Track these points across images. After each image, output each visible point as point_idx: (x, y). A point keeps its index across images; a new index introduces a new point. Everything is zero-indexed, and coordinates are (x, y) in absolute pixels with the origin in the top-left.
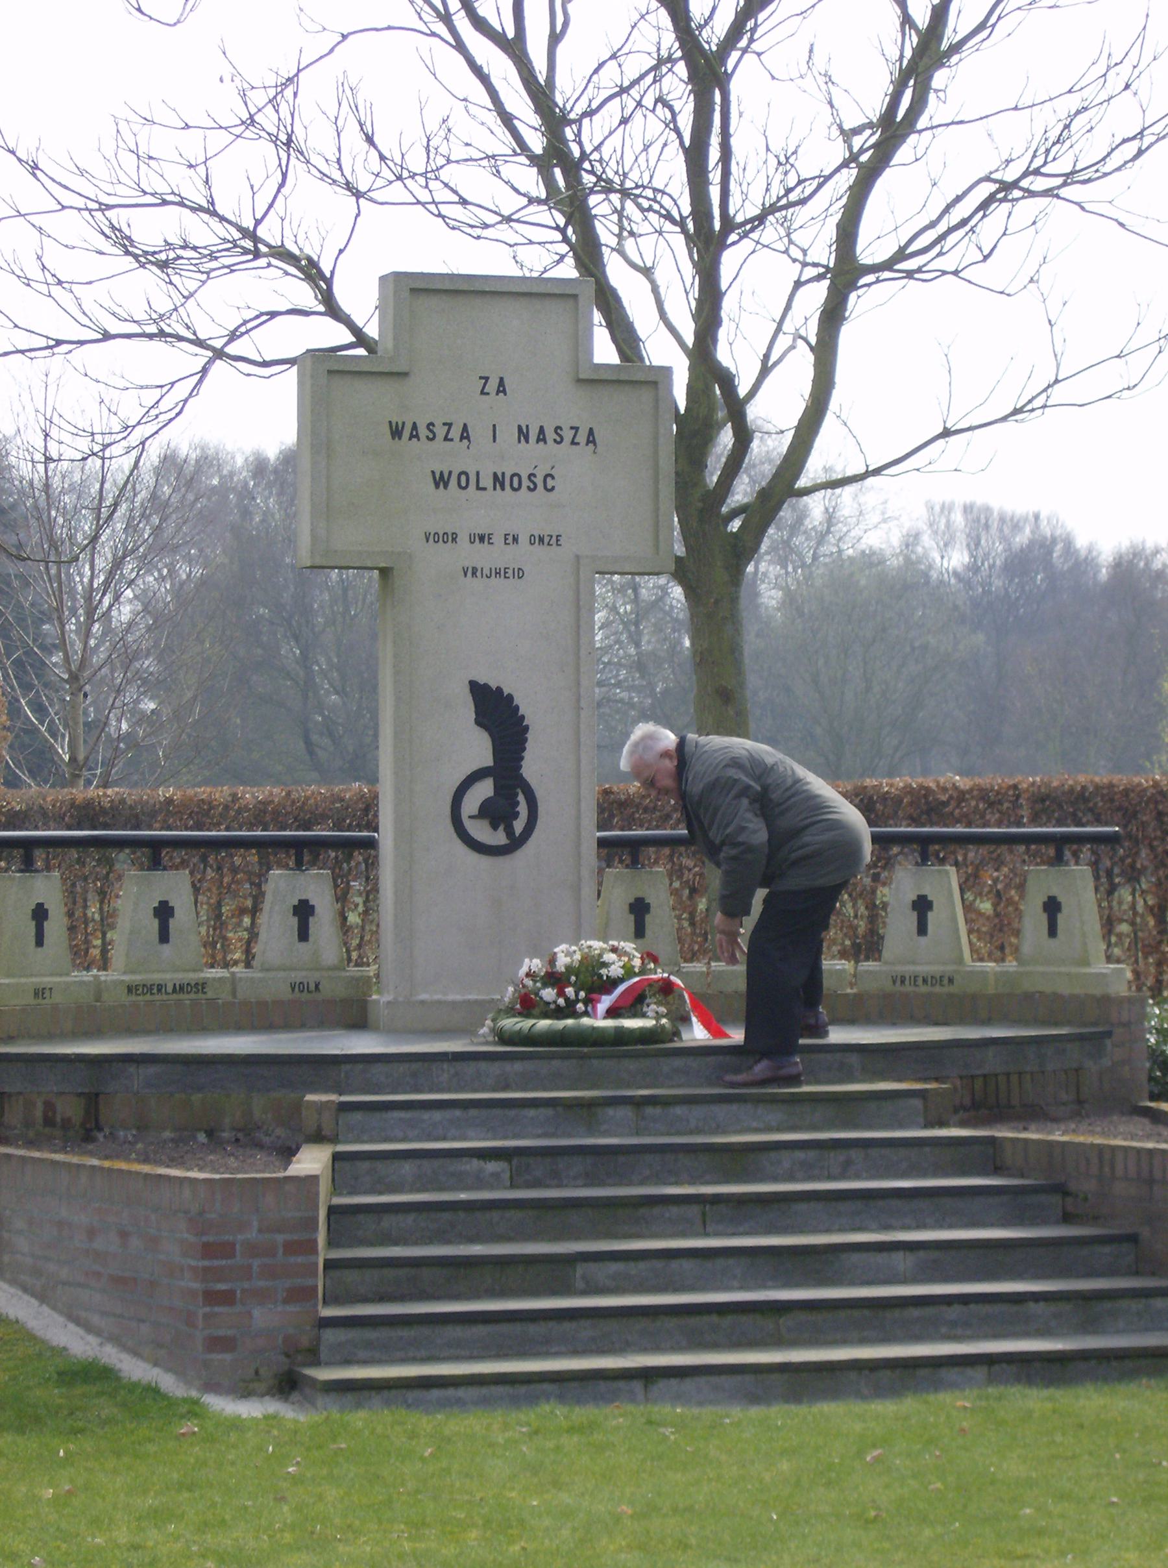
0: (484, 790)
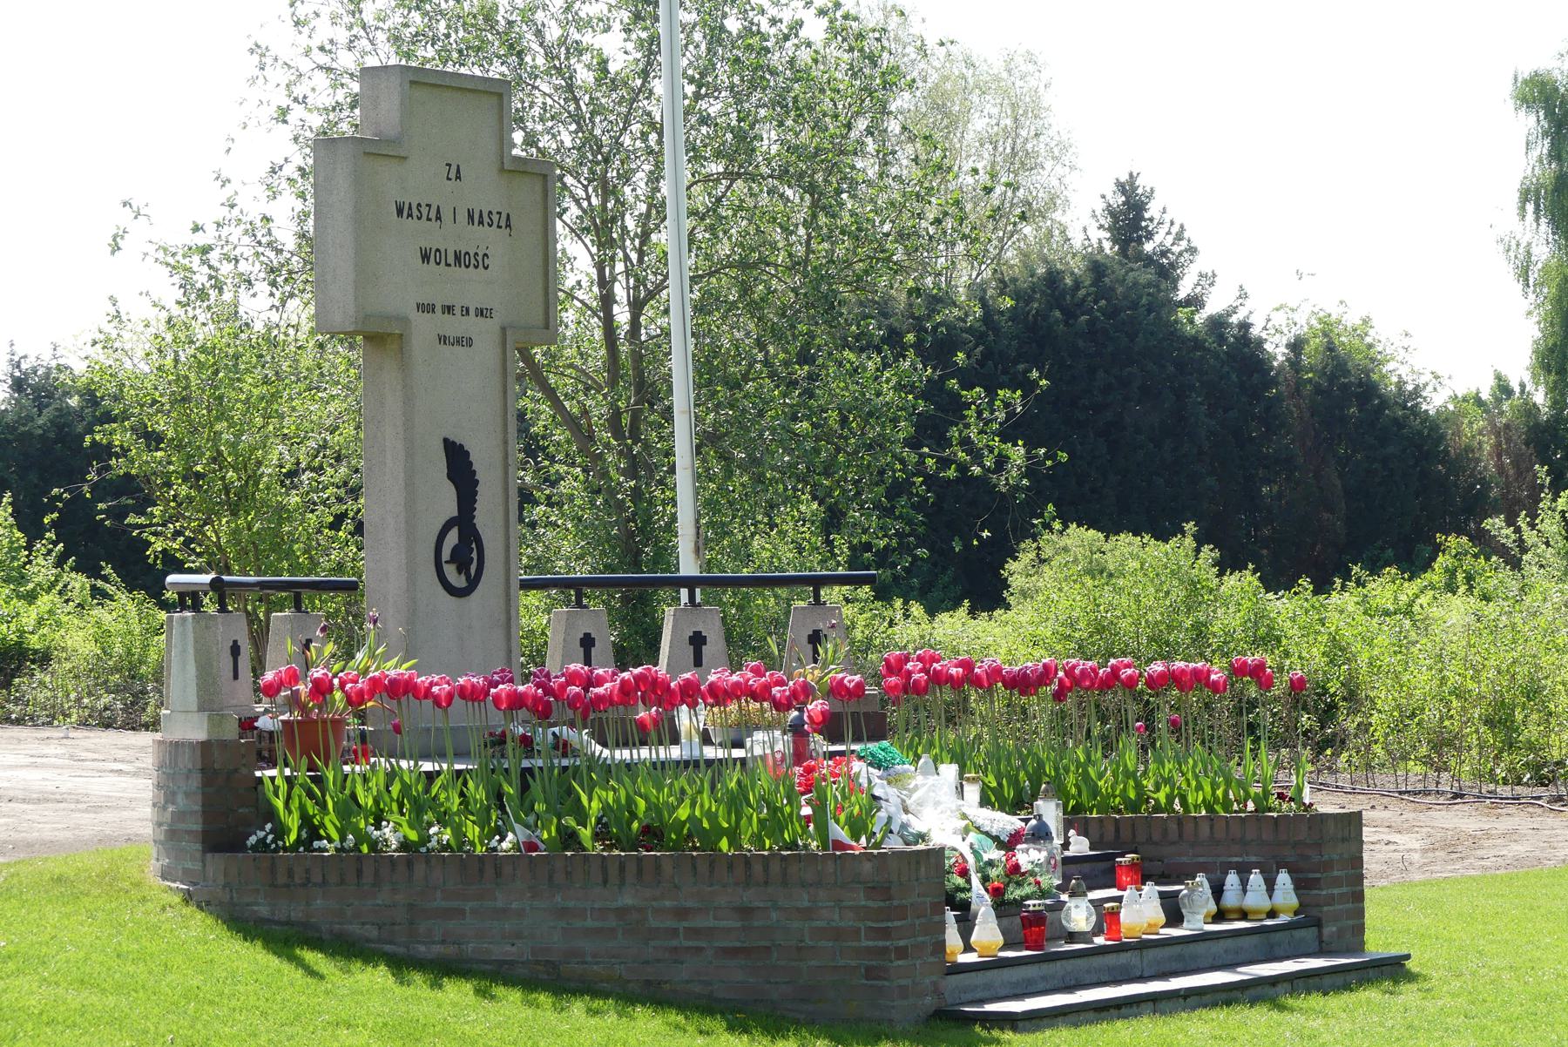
0: (453, 538)
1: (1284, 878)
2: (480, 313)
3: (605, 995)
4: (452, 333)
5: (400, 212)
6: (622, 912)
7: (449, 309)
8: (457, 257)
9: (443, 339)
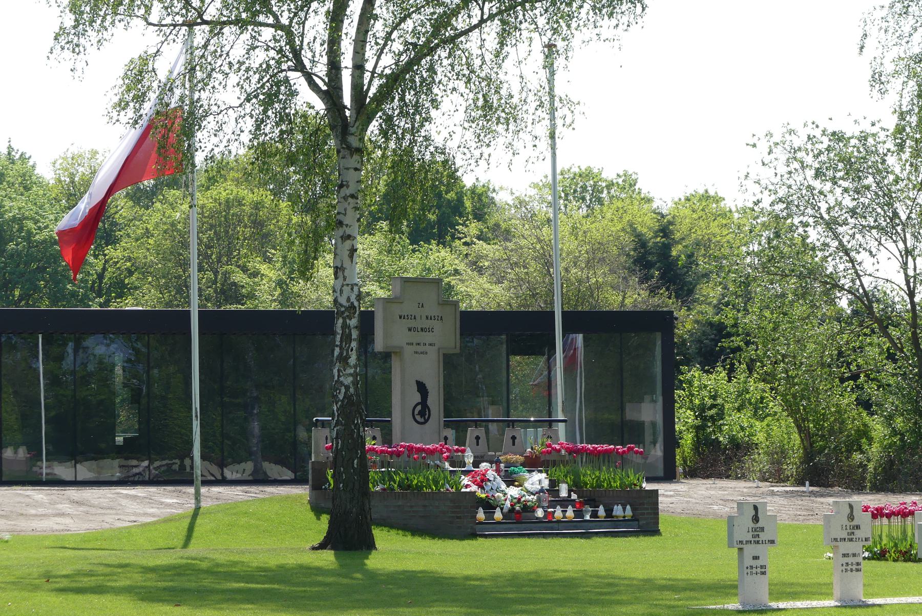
0: (419, 408)
1: (628, 507)
2: (431, 345)
3: (408, 531)
4: (419, 351)
5: (400, 317)
6: (399, 506)
7: (419, 344)
8: (422, 329)
9: (416, 353)
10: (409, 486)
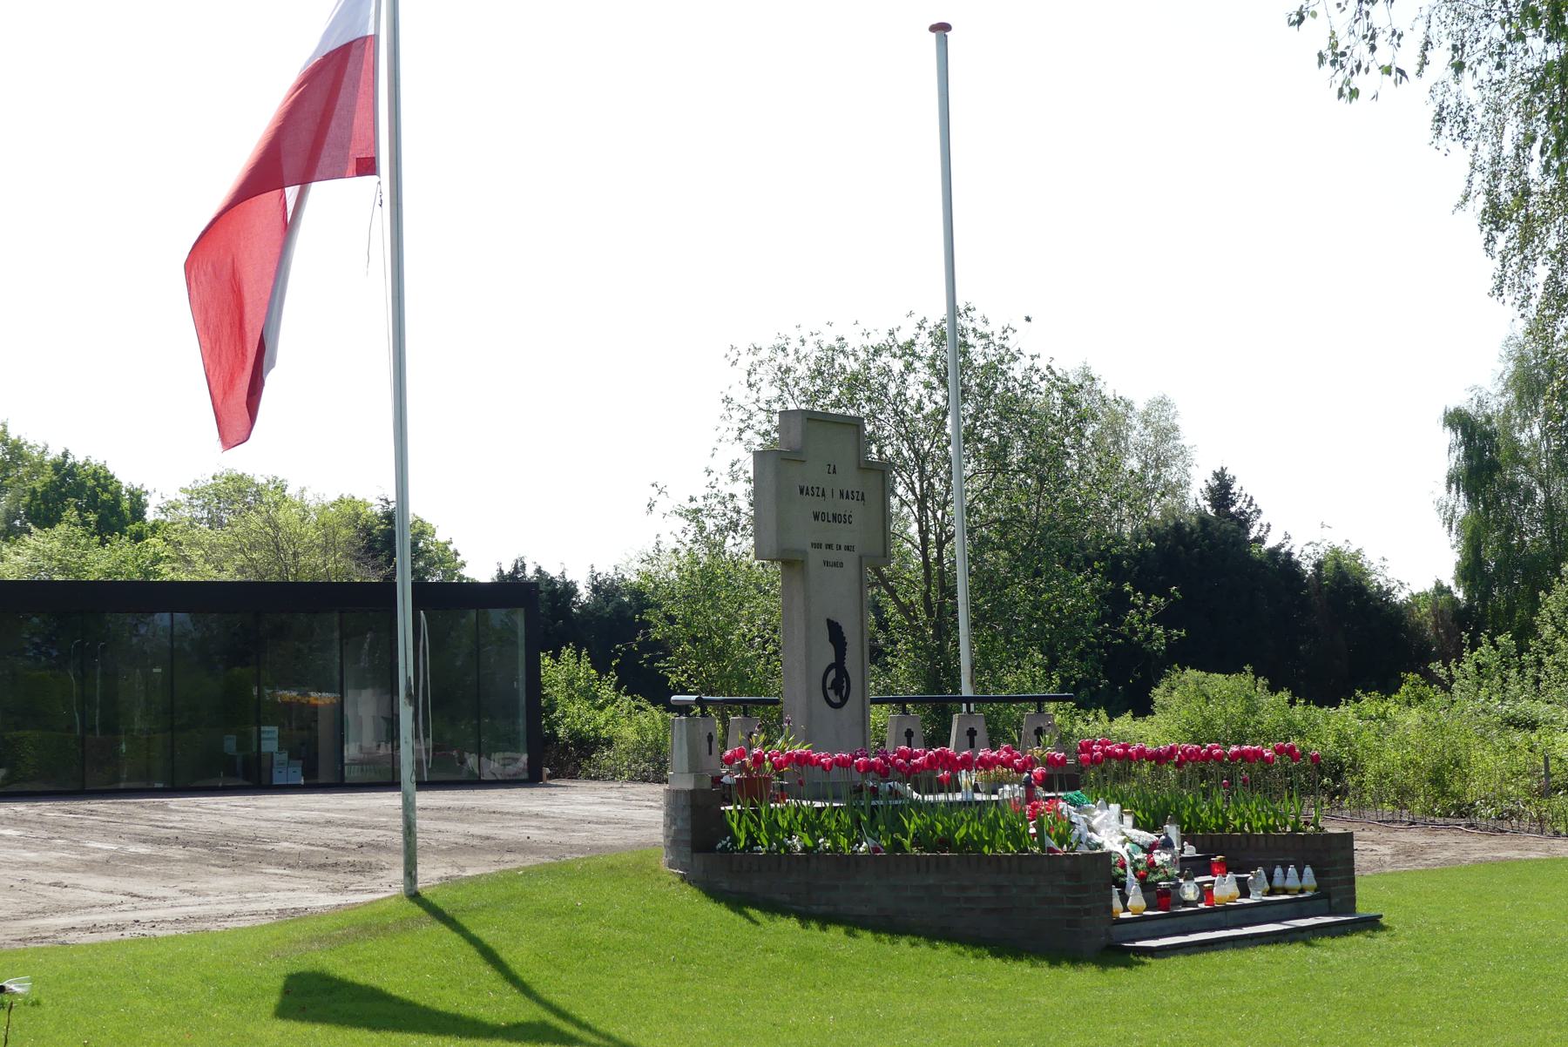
1: (1308, 870)
2: (847, 548)
7: (829, 546)
8: (834, 517)
9: (826, 563)
10: (946, 842)
